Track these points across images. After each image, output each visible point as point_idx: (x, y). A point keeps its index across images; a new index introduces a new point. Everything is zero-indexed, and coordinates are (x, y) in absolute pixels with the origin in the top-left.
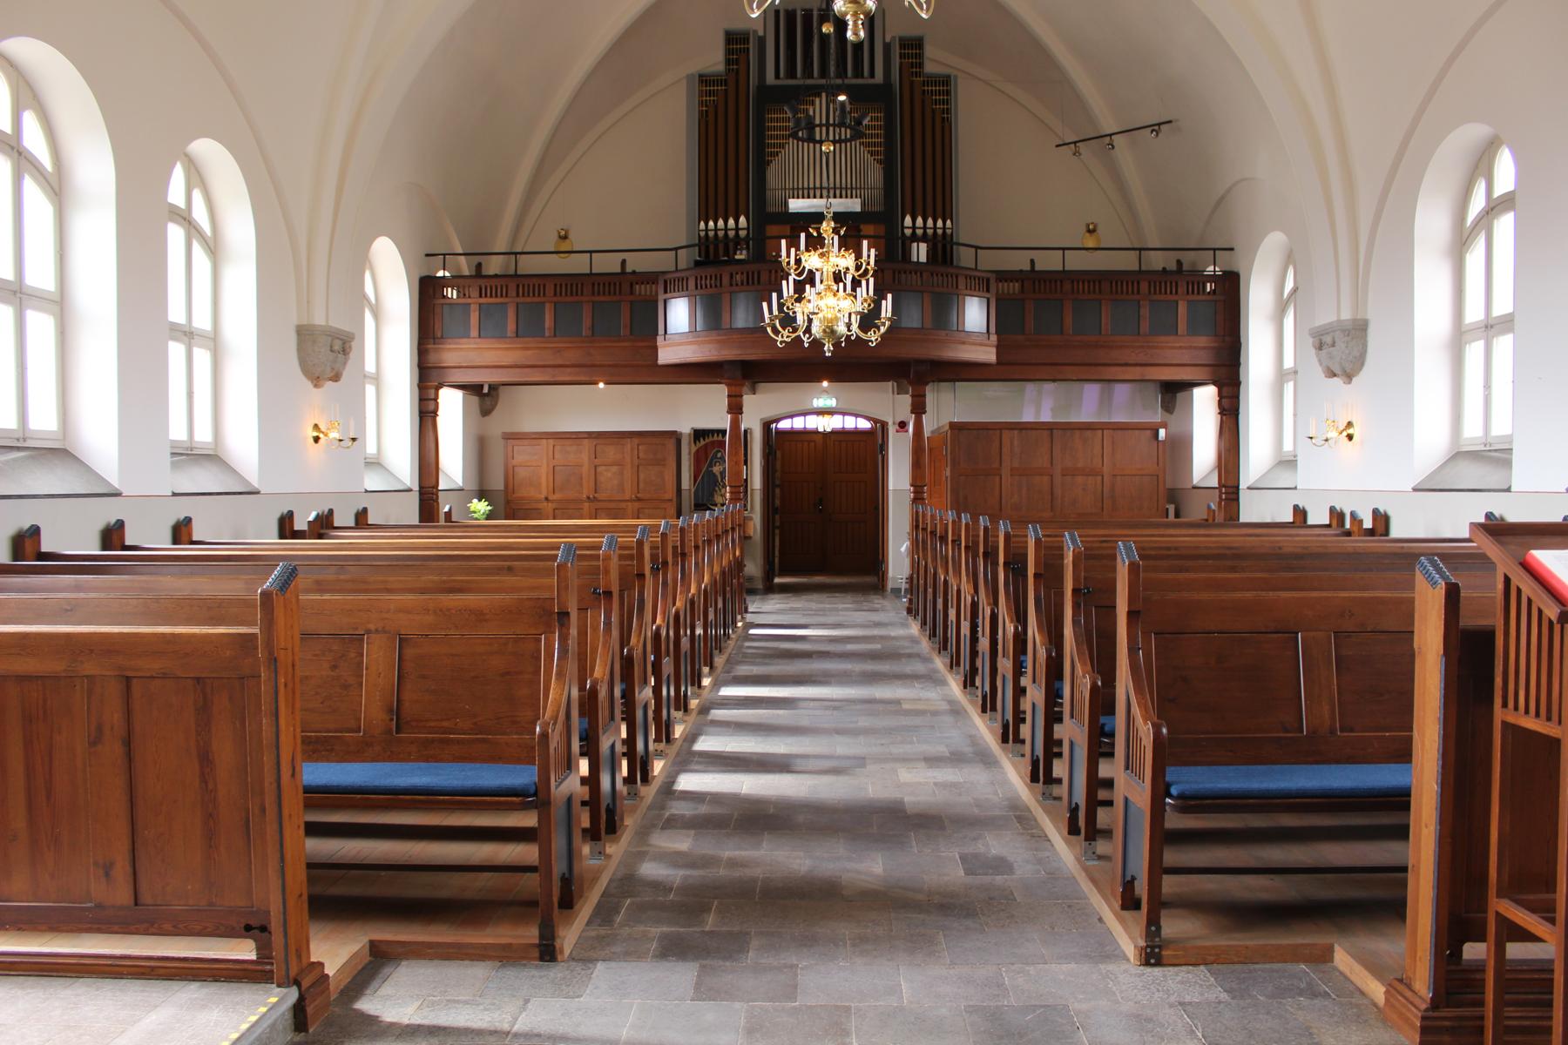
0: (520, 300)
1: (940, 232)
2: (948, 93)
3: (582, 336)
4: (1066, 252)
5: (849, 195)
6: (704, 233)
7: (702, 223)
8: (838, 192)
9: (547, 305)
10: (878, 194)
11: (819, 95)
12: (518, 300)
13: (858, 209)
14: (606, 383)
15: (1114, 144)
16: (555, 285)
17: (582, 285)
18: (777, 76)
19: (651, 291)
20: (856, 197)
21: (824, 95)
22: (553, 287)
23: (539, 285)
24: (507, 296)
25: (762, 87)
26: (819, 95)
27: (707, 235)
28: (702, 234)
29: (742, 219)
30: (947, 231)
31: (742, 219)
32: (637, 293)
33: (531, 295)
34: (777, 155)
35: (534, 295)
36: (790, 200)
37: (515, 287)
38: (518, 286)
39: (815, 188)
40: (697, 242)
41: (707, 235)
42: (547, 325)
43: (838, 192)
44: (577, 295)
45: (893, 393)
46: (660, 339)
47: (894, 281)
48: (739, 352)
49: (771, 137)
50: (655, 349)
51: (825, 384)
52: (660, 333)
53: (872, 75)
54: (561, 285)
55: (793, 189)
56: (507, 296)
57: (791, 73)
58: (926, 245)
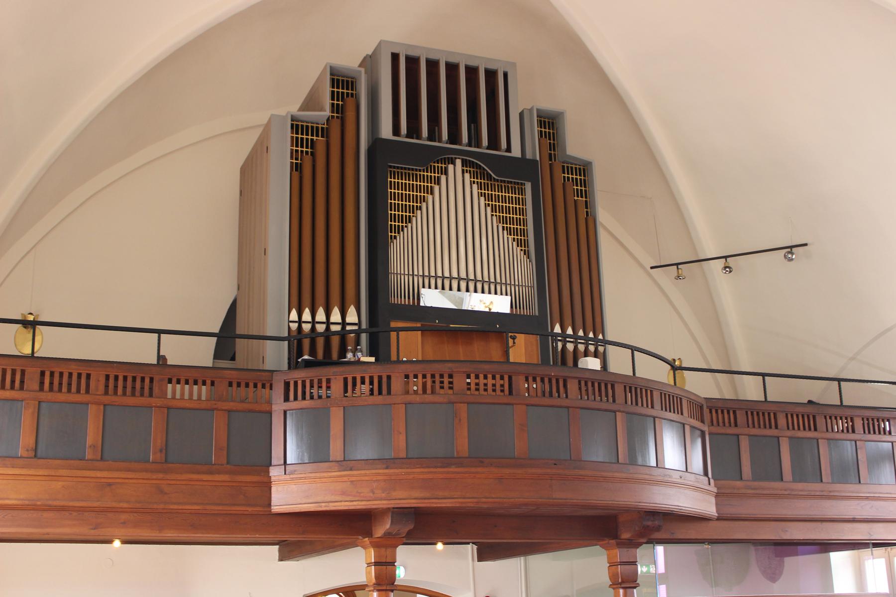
0: (46, 395)
1: (307, 327)
2: (584, 183)
3: (148, 461)
4: (164, 337)
5: (433, 285)
6: (296, 325)
7: (294, 315)
8: (479, 286)
9: (92, 409)
10: (530, 292)
11: (453, 162)
12: (43, 396)
13: (506, 309)
14: (445, 544)
15: (730, 266)
16: (107, 377)
17: (152, 380)
18: (396, 130)
19: (182, 394)
20: (507, 295)
21: (459, 162)
22: (103, 380)
23: (79, 375)
24: (22, 388)
25: (377, 145)
26: (453, 162)
27: (300, 328)
28: (294, 326)
29: (352, 316)
30: (304, 325)
31: (352, 316)
32: (169, 396)
33: (64, 389)
34: (403, 230)
35: (69, 391)
36: (423, 291)
37: (37, 377)
38: (43, 374)
39: (496, 283)
40: (286, 334)
41: (300, 328)
42: (90, 440)
43: (479, 286)
44: (142, 395)
45: (473, 560)
46: (275, 472)
47: (346, 391)
48: (329, 498)
49: (397, 207)
50: (267, 486)
51: (440, 546)
52: (274, 462)
53: (509, 149)
54: (116, 378)
55: (423, 276)
56: (22, 388)
57: (413, 130)
58: (218, 332)
